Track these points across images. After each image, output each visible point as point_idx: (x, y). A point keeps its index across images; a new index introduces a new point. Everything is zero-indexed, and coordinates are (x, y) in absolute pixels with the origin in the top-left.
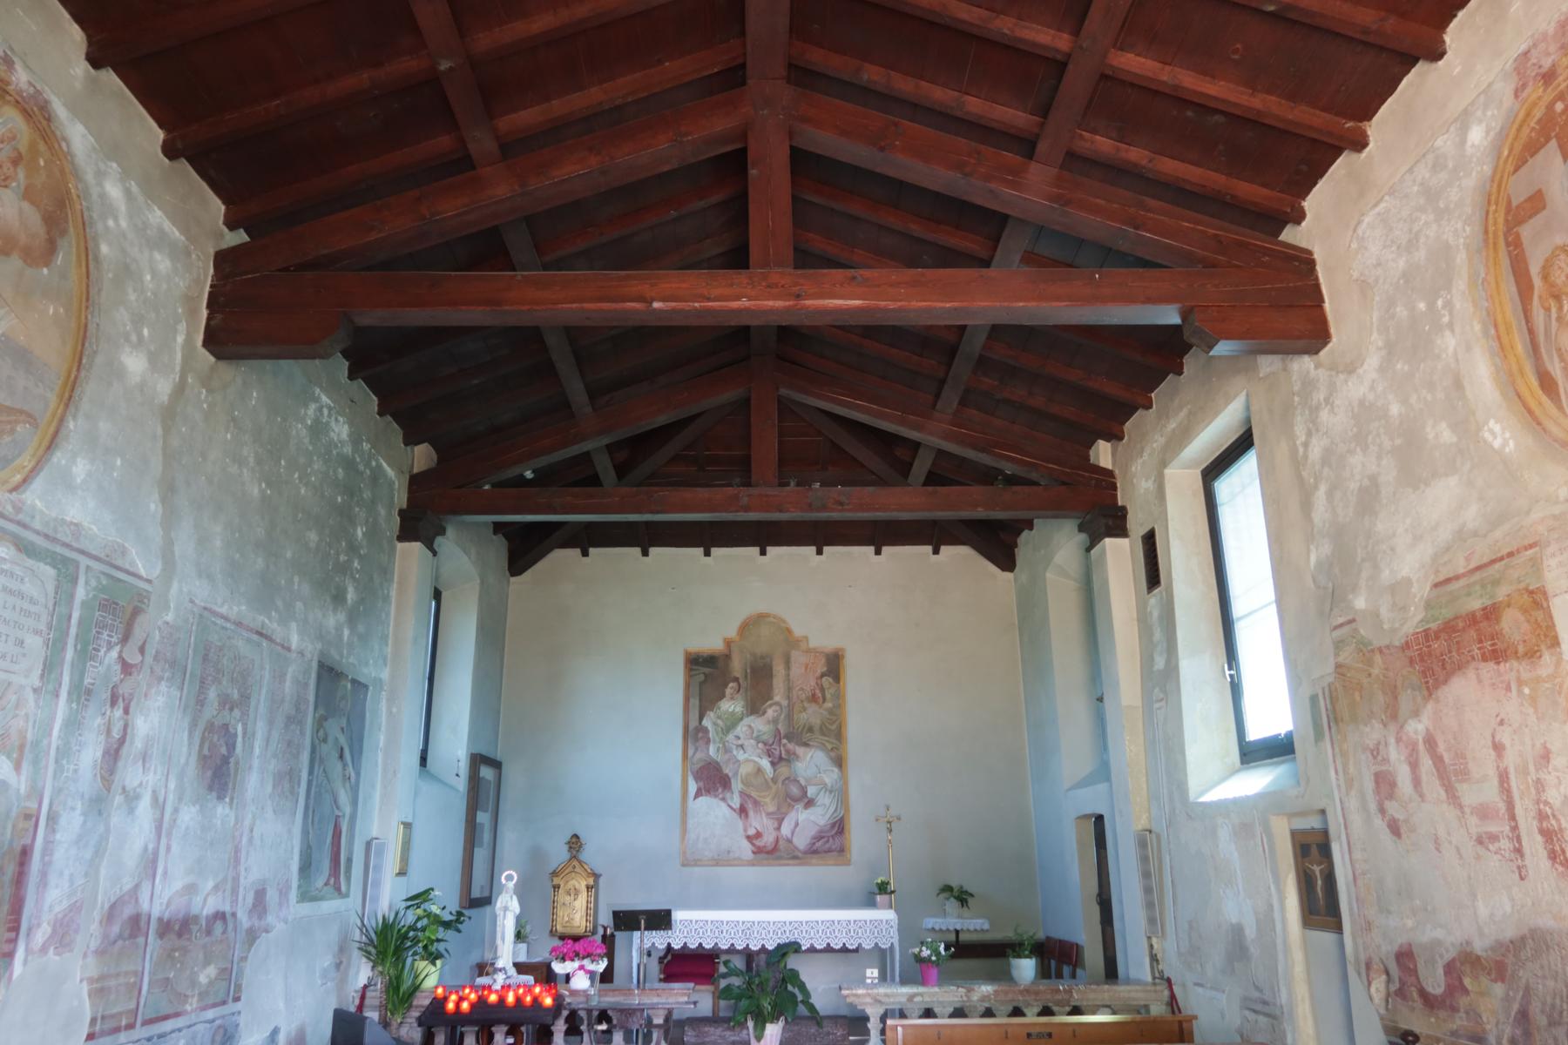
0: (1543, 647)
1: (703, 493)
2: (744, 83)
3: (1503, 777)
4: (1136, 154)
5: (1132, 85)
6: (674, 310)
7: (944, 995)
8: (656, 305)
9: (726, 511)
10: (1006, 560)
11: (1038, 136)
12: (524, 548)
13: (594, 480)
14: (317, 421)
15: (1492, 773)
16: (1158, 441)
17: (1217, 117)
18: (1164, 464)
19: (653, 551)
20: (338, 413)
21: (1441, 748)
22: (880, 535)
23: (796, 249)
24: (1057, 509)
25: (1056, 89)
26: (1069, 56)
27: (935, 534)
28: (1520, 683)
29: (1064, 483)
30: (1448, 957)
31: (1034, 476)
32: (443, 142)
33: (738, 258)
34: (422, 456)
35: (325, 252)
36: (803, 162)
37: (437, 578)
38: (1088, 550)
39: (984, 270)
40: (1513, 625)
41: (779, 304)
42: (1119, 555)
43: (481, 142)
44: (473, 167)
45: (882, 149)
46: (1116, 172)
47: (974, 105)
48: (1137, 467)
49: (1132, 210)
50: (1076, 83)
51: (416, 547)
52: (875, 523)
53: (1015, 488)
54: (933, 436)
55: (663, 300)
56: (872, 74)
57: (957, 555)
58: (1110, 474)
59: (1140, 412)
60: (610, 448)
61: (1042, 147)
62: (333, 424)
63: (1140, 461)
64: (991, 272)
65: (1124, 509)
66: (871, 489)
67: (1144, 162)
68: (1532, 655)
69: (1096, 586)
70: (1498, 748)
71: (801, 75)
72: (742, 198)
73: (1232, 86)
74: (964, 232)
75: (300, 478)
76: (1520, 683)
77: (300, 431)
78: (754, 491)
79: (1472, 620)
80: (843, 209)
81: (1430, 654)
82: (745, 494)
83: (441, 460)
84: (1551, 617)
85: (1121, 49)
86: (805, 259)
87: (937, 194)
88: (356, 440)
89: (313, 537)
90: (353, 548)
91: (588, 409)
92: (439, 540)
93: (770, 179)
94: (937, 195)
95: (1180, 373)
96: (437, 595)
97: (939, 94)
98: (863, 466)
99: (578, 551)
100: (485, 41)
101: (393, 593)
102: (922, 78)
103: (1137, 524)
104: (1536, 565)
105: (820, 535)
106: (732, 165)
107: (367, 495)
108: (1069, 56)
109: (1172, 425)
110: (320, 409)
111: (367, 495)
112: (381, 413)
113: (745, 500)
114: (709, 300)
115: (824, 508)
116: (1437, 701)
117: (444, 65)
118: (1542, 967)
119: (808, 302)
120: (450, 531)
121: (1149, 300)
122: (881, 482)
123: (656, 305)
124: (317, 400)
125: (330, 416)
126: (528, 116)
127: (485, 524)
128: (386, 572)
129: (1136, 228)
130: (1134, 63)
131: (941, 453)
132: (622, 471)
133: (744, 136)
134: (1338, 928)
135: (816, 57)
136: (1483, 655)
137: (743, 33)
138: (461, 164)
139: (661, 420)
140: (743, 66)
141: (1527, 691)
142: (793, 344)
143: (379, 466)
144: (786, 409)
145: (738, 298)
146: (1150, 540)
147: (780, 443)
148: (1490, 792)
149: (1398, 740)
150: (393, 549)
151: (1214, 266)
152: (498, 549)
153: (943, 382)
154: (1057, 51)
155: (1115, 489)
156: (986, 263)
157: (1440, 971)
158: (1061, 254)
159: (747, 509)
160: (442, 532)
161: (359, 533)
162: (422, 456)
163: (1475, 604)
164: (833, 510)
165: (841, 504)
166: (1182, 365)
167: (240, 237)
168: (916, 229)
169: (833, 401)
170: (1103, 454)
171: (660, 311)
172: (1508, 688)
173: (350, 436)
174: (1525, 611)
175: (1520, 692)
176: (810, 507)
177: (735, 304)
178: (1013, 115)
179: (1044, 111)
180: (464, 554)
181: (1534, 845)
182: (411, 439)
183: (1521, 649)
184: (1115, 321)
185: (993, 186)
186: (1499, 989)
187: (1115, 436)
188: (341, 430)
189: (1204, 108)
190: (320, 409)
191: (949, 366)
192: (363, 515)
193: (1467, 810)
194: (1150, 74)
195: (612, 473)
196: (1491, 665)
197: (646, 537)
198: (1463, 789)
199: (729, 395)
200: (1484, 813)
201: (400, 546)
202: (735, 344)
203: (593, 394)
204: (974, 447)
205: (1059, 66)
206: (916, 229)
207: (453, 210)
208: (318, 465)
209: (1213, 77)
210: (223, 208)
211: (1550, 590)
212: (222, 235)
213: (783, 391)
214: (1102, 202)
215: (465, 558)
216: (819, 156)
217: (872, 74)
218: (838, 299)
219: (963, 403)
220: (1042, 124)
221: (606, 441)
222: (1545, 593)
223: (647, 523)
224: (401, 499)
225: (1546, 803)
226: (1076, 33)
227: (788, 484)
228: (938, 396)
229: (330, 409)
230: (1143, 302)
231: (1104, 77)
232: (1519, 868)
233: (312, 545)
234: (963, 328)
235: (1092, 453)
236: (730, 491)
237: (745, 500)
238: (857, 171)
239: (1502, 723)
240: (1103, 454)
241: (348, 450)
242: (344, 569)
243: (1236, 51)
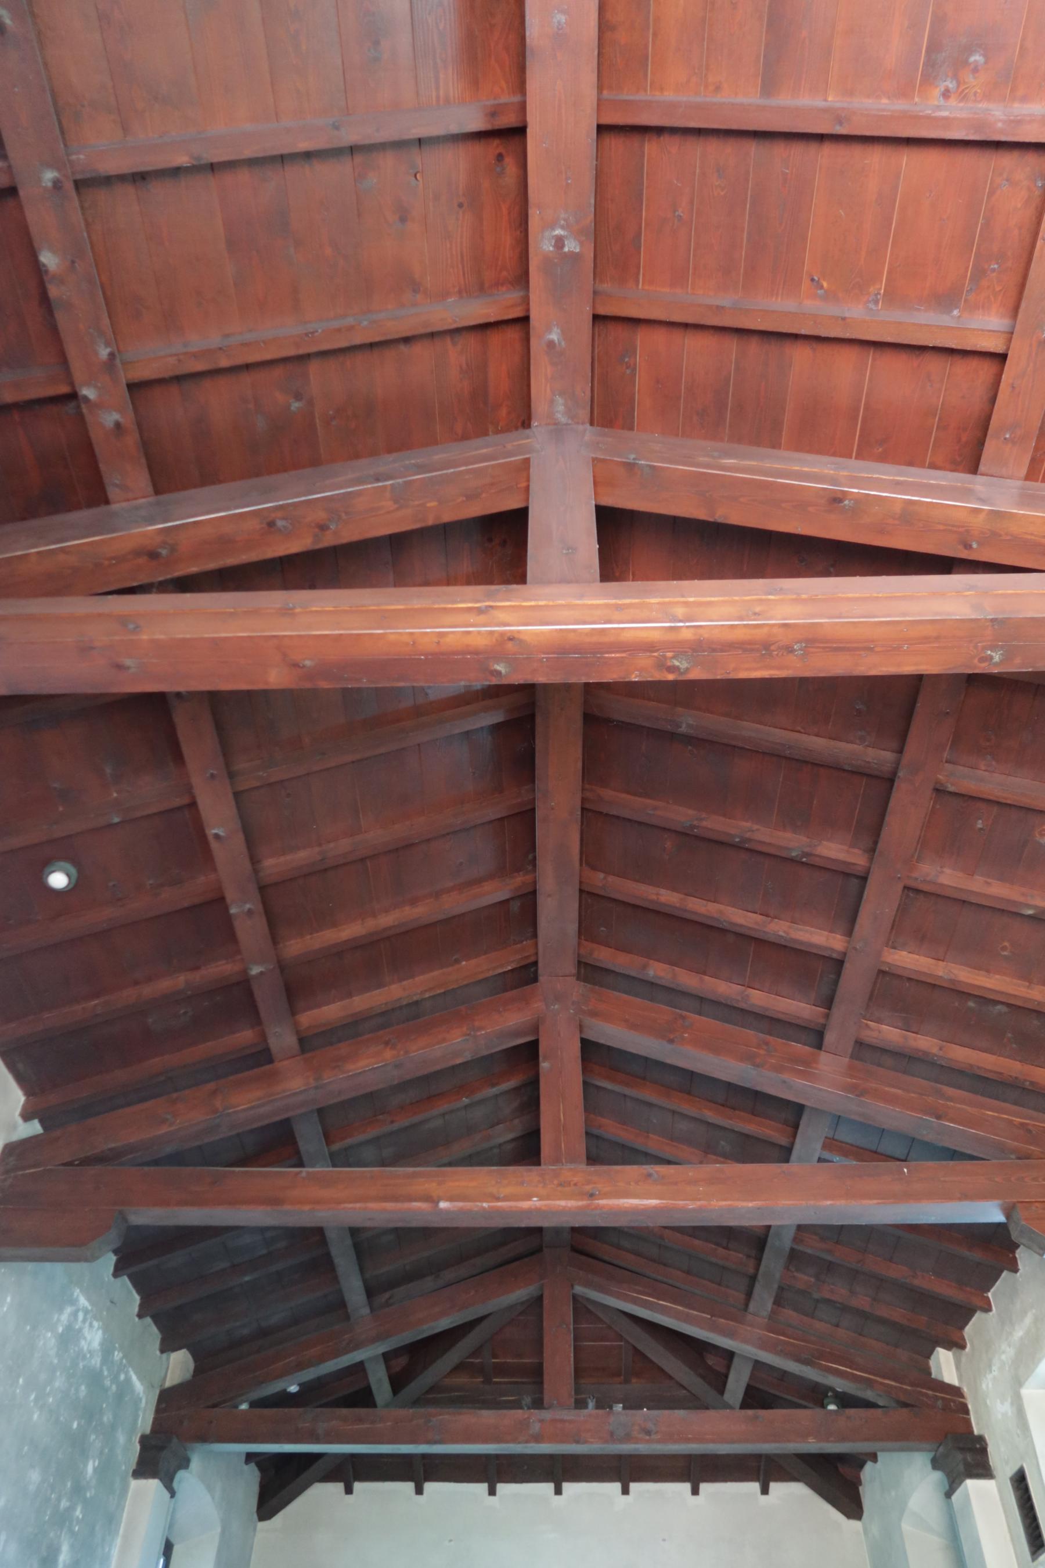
1: (488, 1417)
2: (535, 979)
4: (925, 1043)
5: (910, 979)
6: (461, 1211)
7: (641, 97)
8: (443, 1205)
9: (515, 1440)
10: (850, 1503)
11: (824, 1026)
12: (278, 1483)
13: (363, 1398)
14: (69, 1328)
16: (1005, 1353)
17: (999, 1007)
18: (1018, 1383)
19: (429, 1487)
20: (95, 1318)
22: (698, 1470)
23: (587, 1134)
24: (903, 1438)
25: (836, 982)
26: (845, 954)
27: (764, 1470)
29: (905, 1405)
31: (869, 1395)
32: (245, 1036)
33: (527, 1151)
34: (179, 1365)
35: (113, 1145)
36: (591, 1051)
37: (171, 1526)
38: (948, 1495)
39: (785, 1165)
41: (571, 1204)
42: (986, 1500)
43: (282, 1038)
44: (271, 1061)
45: (671, 1041)
46: (907, 1060)
47: (758, 998)
48: (987, 1384)
49: (930, 1099)
50: (854, 981)
51: (153, 1485)
52: (689, 1458)
53: (851, 1412)
54: (748, 1345)
55: (451, 1199)
56: (657, 971)
57: (791, 1496)
58: (957, 1391)
59: (978, 1316)
60: (387, 1357)
61: (830, 1038)
62: (86, 1331)
63: (989, 1376)
64: (793, 1166)
65: (981, 1439)
66: (681, 1413)
67: (935, 1050)
69: (966, 1549)
71: (590, 972)
72: (534, 1083)
73: (1008, 979)
74: (761, 1127)
75: (36, 1400)
77: (48, 1341)
78: (546, 1415)
80: (635, 1103)
82: (536, 1419)
83: (198, 1371)
85: (895, 948)
86: (601, 1152)
87: (729, 1084)
88: (107, 1351)
89: (35, 1477)
90: (78, 1490)
91: (366, 1311)
92: (181, 1474)
93: (561, 1073)
94: (729, 1085)
95: (1015, 1270)
96: (168, 1550)
97: (724, 988)
98: (671, 1378)
99: (340, 1486)
100: (295, 947)
101: (115, 1552)
102: (704, 973)
103: (1002, 1458)
105: (627, 1470)
106: (526, 1055)
107: (107, 1418)
108: (845, 954)
109: (1019, 1333)
110: (75, 1314)
111: (107, 1418)
112: (140, 1316)
113: (536, 1427)
114: (498, 1199)
115: (628, 1438)
117: (255, 970)
119: (602, 1202)
120: (195, 1463)
121: (965, 1196)
122: (695, 1403)
123: (443, 1205)
124: (73, 1302)
125: (84, 1321)
126: (330, 1011)
127: (239, 1454)
128: (111, 1521)
129: (939, 1117)
130: (907, 959)
131: (758, 1364)
132: (398, 1383)
133: (535, 1028)
135: (603, 956)
137: (535, 935)
138: (261, 1057)
139: (444, 1324)
140: (535, 963)
142: (588, 1246)
143: (128, 1380)
144: (582, 1309)
145: (528, 1197)
146: (1020, 1481)
147: (577, 1349)
150: (125, 1489)
151: (1028, 1158)
152: (251, 1479)
153: (753, 1278)
154: (832, 950)
155: (967, 1412)
156: (785, 1154)
158: (869, 1150)
159: (537, 1439)
160: (185, 1463)
161: (90, 1469)
162: (179, 1365)
164: (637, 1441)
165: (648, 1433)
166: (1015, 1260)
167: (35, 1128)
168: (710, 1115)
169: (635, 1301)
170: (945, 1365)
171: (447, 1211)
173: (102, 1344)
176: (612, 1437)
177: (525, 1205)
178: (798, 1007)
179: (828, 1003)
180: (211, 1486)
182: (168, 1346)
184: (932, 1220)
185: (785, 1076)
187: (957, 1344)
188: (93, 1337)
189: (985, 1000)
190: (75, 1314)
191: (759, 1260)
192: (98, 1444)
194: (925, 970)
195: (387, 1386)
197: (419, 1471)
199: (520, 1294)
201: (135, 1484)
202: (521, 1247)
203: (370, 1293)
204: (798, 1360)
205: (838, 964)
206: (710, 1115)
207: (247, 1105)
208: (59, 1383)
209: (988, 971)
210: (22, 1099)
212: (14, 1127)
213: (579, 1289)
214: (899, 1092)
215: (208, 1498)
216: (610, 1048)
217: (657, 971)
218: (633, 1198)
219: (778, 1302)
220: (827, 1016)
221: (382, 1348)
223: (424, 1456)
224: (145, 1422)
226: (849, 933)
227: (586, 1407)
228: (749, 1295)
229: (86, 1312)
230: (960, 1199)
231: (881, 973)
233: (32, 1488)
234: (769, 1227)
235: (932, 1363)
236: (519, 1414)
237: (536, 1427)
238: (647, 1062)
240: (945, 1365)
241: (96, 1361)
242: (62, 1519)
243: (1004, 948)
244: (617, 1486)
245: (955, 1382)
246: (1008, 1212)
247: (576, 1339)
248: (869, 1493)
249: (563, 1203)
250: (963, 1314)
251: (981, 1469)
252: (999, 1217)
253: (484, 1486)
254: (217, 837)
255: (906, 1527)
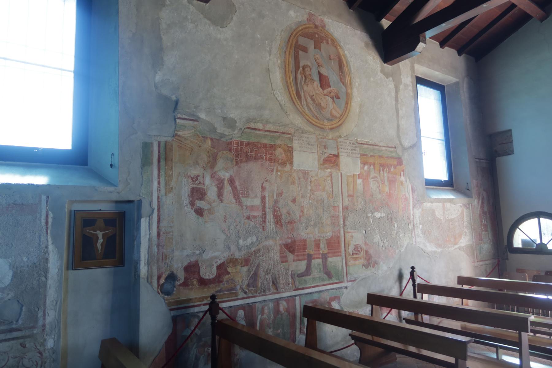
0: (288, 163)
3: (263, 199)
15: (259, 195)
21: (237, 184)
28: (277, 170)
30: (219, 262)
40: (279, 153)
68: (283, 164)
70: (263, 188)
76: (277, 170)
79: (265, 146)
81: (241, 150)
84: (293, 156)
104: (291, 140)
116: (240, 167)
118: (266, 257)
134: (103, 259)
136: (266, 158)
141: (279, 173)
148: (257, 202)
149: (212, 177)
157: (215, 268)
163: (266, 141)
172: (272, 171)
174: (284, 151)
175: (277, 173)
181: (270, 217)
183: (280, 161)
186: (245, 269)
193: (245, 207)
196: (268, 162)
198: (243, 200)
200: (252, 208)
211: (294, 148)
222: (292, 149)
225: (278, 207)
232: (263, 227)
239: (267, 181)
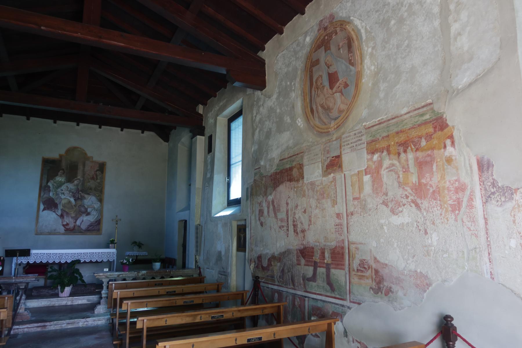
8: (42, 28)
18: (217, 115)
27: (143, 127)
38: (192, 138)
41: (93, 38)
48: (210, 115)
55: (45, 26)
103: (207, 132)
109: (221, 104)
123: (42, 28)
145: (77, 33)
146: (210, 138)
170: (200, 109)
177: (76, 35)
187: (204, 104)
197: (29, 113)
218: (116, 42)
240: (200, 109)
244: (98, 126)
245: (202, 113)
246: (228, 71)
247: (515, 220)
248: (172, 137)
249: (90, 37)
250: (209, 97)
251: (202, 134)
252: (224, 72)
253: (120, 129)
254: (288, 154)
255: (179, 145)
